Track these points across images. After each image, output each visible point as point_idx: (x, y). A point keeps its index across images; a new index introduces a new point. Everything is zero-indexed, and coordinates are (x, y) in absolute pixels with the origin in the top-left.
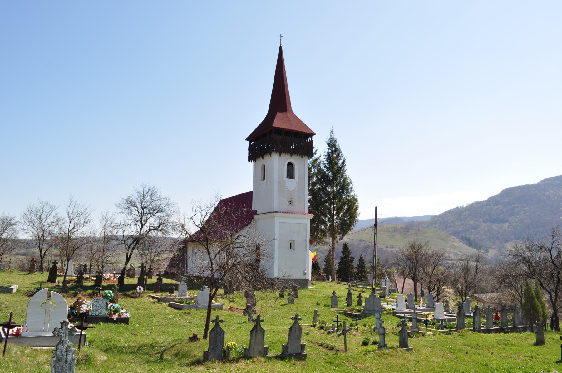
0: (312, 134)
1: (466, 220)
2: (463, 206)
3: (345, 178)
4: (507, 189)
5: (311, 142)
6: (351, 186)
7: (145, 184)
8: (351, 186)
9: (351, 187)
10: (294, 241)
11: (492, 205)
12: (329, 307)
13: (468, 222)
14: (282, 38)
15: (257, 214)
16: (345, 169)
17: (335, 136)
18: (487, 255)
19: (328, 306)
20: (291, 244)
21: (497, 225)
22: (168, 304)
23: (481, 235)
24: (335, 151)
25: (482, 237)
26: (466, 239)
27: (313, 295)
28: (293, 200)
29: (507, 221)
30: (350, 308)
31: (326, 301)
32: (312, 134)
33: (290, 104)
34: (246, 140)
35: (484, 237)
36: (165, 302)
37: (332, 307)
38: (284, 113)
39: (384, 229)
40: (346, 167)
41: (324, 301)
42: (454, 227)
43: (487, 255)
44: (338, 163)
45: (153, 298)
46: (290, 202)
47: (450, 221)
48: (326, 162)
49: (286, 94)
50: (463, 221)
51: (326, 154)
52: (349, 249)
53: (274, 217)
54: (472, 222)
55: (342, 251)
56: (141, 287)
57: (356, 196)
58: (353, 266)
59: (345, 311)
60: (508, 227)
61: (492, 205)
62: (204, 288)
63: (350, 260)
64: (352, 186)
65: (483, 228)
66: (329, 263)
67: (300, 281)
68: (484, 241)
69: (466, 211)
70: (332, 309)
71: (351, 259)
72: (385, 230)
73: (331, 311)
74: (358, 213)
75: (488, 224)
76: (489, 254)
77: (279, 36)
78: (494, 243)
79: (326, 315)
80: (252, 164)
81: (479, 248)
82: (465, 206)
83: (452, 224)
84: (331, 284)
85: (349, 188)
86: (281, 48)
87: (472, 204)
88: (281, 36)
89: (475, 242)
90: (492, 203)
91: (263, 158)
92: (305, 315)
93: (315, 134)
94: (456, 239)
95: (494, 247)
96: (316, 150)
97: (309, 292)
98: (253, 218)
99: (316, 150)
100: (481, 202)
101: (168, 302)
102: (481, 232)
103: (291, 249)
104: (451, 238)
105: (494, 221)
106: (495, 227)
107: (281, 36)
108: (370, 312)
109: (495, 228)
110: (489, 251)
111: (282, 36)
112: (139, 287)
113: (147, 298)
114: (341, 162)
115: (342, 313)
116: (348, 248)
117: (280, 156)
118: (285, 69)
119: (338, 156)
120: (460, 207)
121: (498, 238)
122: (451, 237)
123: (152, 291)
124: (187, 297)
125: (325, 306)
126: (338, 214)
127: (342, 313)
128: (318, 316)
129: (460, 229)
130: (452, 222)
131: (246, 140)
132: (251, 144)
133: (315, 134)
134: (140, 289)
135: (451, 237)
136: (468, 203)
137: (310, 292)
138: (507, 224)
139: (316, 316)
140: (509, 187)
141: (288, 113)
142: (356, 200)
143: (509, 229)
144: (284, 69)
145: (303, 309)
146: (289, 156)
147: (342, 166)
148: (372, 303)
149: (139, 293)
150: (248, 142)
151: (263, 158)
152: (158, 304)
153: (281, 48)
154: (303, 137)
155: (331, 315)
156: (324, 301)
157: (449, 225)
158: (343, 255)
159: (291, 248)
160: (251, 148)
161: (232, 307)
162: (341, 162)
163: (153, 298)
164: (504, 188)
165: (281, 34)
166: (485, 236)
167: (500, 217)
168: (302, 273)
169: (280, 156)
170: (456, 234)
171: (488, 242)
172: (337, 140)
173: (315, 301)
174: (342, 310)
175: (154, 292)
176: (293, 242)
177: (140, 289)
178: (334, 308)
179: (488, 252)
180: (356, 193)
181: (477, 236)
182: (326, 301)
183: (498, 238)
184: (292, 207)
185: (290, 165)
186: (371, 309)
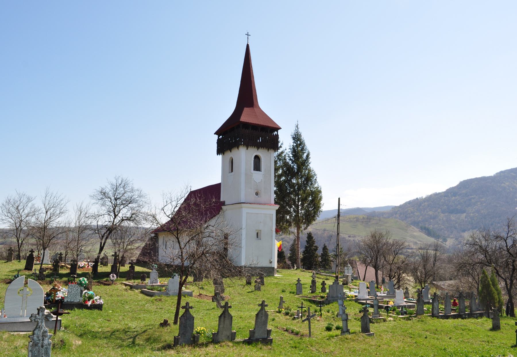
0: (277, 129)
1: (426, 211)
2: (422, 197)
3: (310, 171)
4: (464, 181)
5: (277, 136)
6: (315, 178)
7: (118, 176)
8: (315, 178)
9: (315, 179)
10: (261, 230)
11: (450, 196)
12: (294, 294)
13: (427, 212)
14: (249, 36)
15: (225, 205)
16: (309, 162)
17: (300, 130)
18: (445, 244)
19: (293, 293)
20: (257, 233)
21: (455, 215)
22: (140, 291)
23: (439, 225)
24: (300, 144)
25: (440, 226)
26: (425, 228)
27: (279, 282)
28: (260, 191)
29: (464, 212)
30: (314, 295)
31: (291, 288)
32: (277, 129)
33: (257, 100)
34: (215, 134)
35: (443, 227)
36: (137, 289)
37: (297, 294)
38: (251, 108)
39: (347, 219)
40: (310, 160)
41: (289, 288)
42: (414, 217)
43: (445, 244)
44: (303, 156)
45: (126, 285)
46: (257, 194)
47: (410, 212)
48: (291, 155)
49: (253, 90)
50: (422, 212)
51: (291, 148)
52: (313, 239)
53: (242, 208)
54: (431, 213)
55: (306, 241)
56: (114, 275)
57: (320, 188)
58: (317, 254)
59: (309, 298)
60: (466, 218)
61: (450, 196)
62: (175, 276)
63: (314, 249)
64: (316, 178)
65: (441, 219)
66: (294, 252)
67: (266, 269)
68: (442, 231)
69: (425, 202)
70: (297, 296)
71: (315, 248)
72: (348, 220)
73: (296, 298)
74: (322, 204)
75: (446, 214)
76: (447, 243)
77: (246, 34)
78: (452, 232)
79: (291, 301)
80: (220, 157)
81: (437, 237)
82: (424, 197)
83: (412, 215)
84: (296, 272)
85: (313, 180)
86: (248, 46)
87: (431, 195)
88: (248, 35)
89: (433, 232)
90: (450, 194)
91: (231, 151)
92: (271, 302)
93: (280, 128)
94: (416, 229)
95: (452, 236)
96: (282, 144)
97: (275, 279)
98: (221, 209)
99: (282, 144)
100: (439, 193)
101: (140, 289)
102: (439, 222)
103: (258, 239)
104: (411, 228)
105: (452, 212)
106: (453, 217)
107: (248, 35)
108: (333, 299)
109: (453, 218)
110: (447, 240)
111: (249, 34)
112: (112, 274)
113: (120, 285)
114: (305, 155)
115: (306, 300)
116: (312, 238)
117: (247, 149)
118: (252, 66)
119: (303, 149)
120: (420, 198)
121: (456, 228)
122: (411, 227)
123: (124, 279)
124: (159, 284)
125: (290, 293)
126: (302, 205)
127: (306, 300)
128: (284, 302)
129: (420, 219)
130: (412, 212)
131: (215, 134)
132: (220, 137)
133: (280, 128)
134: (113, 276)
135: (411, 227)
136: (427, 194)
137: (276, 279)
138: (465, 214)
139: (282, 302)
140: (466, 179)
141: (255, 108)
142: (320, 192)
143: (466, 219)
144: (251, 66)
145: (269, 296)
146: (256, 149)
147: (306, 159)
148: (335, 290)
149: (112, 281)
150: (217, 136)
151: (231, 151)
152: (130, 291)
153: (248, 46)
154: (269, 131)
155: (296, 302)
156: (289, 288)
157: (408, 215)
158: (307, 244)
159: (257, 237)
160: (219, 142)
161: (202, 294)
162: (305, 155)
163: (126, 285)
164: (462, 180)
165: (248, 33)
166: (443, 225)
167: (457, 207)
168: (268, 262)
169: (247, 149)
170: (415, 224)
171: (446, 232)
172: (302, 134)
173: (281, 288)
174: (306, 297)
175: (127, 280)
176: (259, 231)
177: (113, 276)
178: (298, 294)
179: (446, 242)
180: (320, 185)
181: (436, 226)
182: (291, 288)
183: (456, 228)
184: (259, 198)
185: (257, 158)
186: (335, 296)
